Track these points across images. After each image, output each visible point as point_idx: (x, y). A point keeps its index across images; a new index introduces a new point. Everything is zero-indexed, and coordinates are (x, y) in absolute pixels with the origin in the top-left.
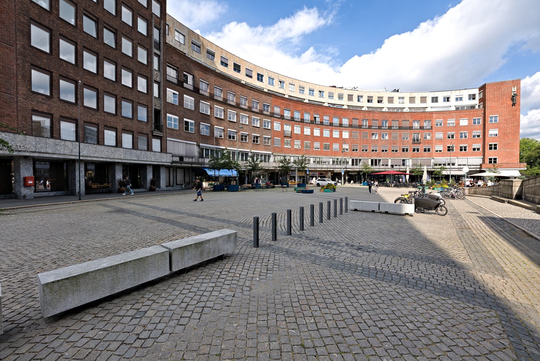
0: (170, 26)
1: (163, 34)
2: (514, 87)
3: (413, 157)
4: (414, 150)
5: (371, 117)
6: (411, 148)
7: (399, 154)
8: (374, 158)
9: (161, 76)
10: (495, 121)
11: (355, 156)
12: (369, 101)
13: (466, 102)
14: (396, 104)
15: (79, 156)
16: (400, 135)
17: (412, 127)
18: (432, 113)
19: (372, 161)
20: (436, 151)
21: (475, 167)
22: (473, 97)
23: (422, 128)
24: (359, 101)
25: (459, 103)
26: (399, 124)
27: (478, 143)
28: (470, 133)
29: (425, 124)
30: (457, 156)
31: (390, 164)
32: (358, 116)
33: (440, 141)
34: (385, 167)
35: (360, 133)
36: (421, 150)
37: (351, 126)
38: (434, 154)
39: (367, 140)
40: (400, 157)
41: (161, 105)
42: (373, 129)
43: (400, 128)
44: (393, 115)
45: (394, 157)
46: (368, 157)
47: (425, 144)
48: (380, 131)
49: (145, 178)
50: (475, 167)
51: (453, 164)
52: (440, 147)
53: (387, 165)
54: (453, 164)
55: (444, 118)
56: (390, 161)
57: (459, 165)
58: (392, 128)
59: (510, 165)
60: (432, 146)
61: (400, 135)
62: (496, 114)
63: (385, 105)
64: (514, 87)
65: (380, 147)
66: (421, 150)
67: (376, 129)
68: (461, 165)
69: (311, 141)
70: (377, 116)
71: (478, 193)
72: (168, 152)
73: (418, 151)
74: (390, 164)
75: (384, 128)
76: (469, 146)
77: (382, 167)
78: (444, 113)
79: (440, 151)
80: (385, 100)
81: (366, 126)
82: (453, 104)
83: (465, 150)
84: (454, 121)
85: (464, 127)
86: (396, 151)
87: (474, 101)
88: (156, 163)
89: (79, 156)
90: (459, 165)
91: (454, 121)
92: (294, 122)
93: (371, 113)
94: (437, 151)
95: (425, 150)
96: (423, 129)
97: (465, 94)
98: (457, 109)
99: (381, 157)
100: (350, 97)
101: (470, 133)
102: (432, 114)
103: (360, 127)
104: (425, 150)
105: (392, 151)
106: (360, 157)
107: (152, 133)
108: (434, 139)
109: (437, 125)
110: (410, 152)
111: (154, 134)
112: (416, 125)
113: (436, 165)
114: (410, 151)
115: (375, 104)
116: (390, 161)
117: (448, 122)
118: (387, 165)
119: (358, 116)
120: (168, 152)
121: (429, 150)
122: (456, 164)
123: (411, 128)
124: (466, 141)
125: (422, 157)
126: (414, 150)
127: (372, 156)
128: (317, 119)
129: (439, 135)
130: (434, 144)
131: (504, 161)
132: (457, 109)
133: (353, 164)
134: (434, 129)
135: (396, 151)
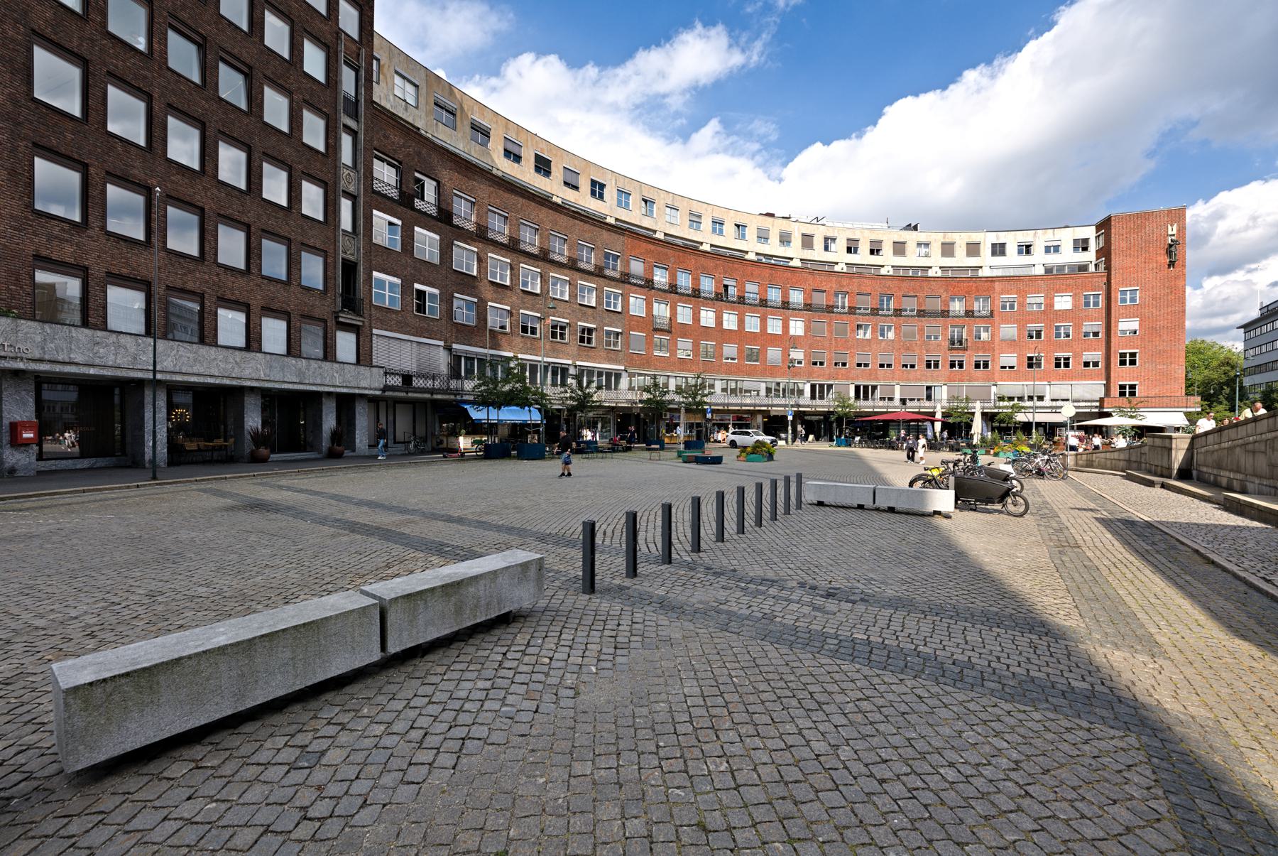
0: (382, 62)
1: (366, 81)
2: (1172, 225)
3: (950, 380)
4: (952, 365)
8: (862, 383)
9: (359, 181)
10: (1133, 300)
13: (1069, 256)
14: (912, 258)
15: (155, 371)
16: (921, 330)
18: (991, 280)
20: (1002, 367)
21: (1089, 404)
23: (969, 314)
24: (826, 249)
25: (1053, 259)
26: (919, 304)
27: (1095, 350)
28: (1078, 326)
29: (977, 306)
30: (1047, 378)
31: (897, 396)
33: (1011, 344)
34: (886, 403)
35: (829, 324)
38: (997, 375)
40: (920, 380)
41: (359, 250)
43: (922, 313)
45: (908, 380)
47: (977, 350)
48: (874, 319)
50: (1089, 404)
52: (1009, 359)
53: (891, 399)
54: (1041, 398)
55: (1019, 292)
56: (897, 388)
57: (1052, 400)
61: (921, 330)
62: (1134, 285)
63: (887, 260)
64: (1172, 225)
65: (875, 357)
69: (716, 341)
70: (867, 286)
74: (897, 396)
75: (885, 312)
76: (1074, 357)
77: (881, 403)
78: (1020, 281)
79: (1010, 367)
83: (1067, 365)
84: (1042, 300)
85: (1064, 314)
86: (912, 366)
87: (1085, 253)
88: (345, 390)
89: (155, 371)
90: (1052, 400)
91: (1042, 300)
94: (1005, 367)
95: (977, 366)
97: (1066, 237)
98: (1049, 270)
99: (877, 379)
100: (807, 241)
101: (1078, 326)
102: (992, 281)
103: (830, 309)
104: (977, 366)
105: (904, 366)
106: (829, 379)
107: (337, 317)
108: (997, 340)
109: (1004, 307)
110: (944, 368)
111: (341, 319)
112: (957, 307)
113: (1001, 399)
115: (863, 257)
117: (1028, 301)
118: (891, 399)
122: (1047, 398)
123: (945, 314)
127: (857, 378)
129: (1009, 331)
130: (996, 352)
132: (1049, 270)
133: (813, 397)
134: (996, 318)
135: (912, 366)
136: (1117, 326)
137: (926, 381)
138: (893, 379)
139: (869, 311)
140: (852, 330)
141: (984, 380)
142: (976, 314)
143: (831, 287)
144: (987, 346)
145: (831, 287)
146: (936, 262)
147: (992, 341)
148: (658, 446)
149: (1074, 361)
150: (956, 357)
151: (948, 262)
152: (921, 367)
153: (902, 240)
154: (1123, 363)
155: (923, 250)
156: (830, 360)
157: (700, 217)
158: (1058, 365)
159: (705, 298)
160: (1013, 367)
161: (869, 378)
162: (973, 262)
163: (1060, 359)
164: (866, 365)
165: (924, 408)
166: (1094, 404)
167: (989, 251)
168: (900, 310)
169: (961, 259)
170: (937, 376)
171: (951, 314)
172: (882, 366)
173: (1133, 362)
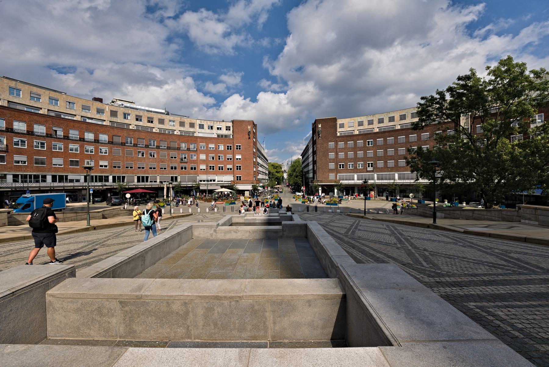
3: (181, 174)
4: (182, 168)
5: (137, 135)
6: (179, 166)
7: (167, 171)
8: (141, 175)
11: (117, 173)
12: (137, 120)
13: (224, 132)
14: (167, 126)
15: (2, 180)
16: (169, 155)
17: (180, 148)
18: (197, 137)
19: (139, 178)
20: (201, 169)
21: (228, 183)
22: (228, 128)
23: (188, 149)
24: (125, 118)
25: (219, 132)
26: (168, 144)
28: (225, 156)
29: (192, 147)
30: (216, 174)
31: (158, 181)
32: (119, 133)
33: (203, 162)
34: (153, 183)
35: (123, 151)
36: (188, 169)
37: (111, 143)
38: (199, 172)
39: (132, 158)
40: (168, 174)
42: (139, 147)
43: (169, 148)
44: (161, 136)
45: (163, 174)
46: (133, 174)
47: (191, 163)
48: (147, 149)
49: (307, 135)
50: (228, 183)
51: (214, 181)
52: (203, 167)
53: (156, 182)
54: (214, 181)
56: (158, 177)
57: (218, 181)
58: (161, 147)
59: (247, 181)
60: (197, 165)
61: (169, 155)
63: (156, 127)
65: (147, 165)
66: (188, 169)
67: (142, 147)
68: (219, 181)
69: (47, 156)
70: (142, 135)
71: (514, 221)
72: (366, 201)
73: (185, 168)
74: (158, 181)
75: (152, 147)
76: (224, 167)
77: (151, 183)
79: (204, 170)
80: (156, 121)
81: (131, 143)
82: (214, 133)
83: (222, 169)
84: (214, 146)
86: (165, 169)
87: (230, 131)
90: (218, 181)
91: (214, 146)
92: (13, 134)
93: (136, 132)
94: (202, 169)
95: (192, 169)
96: (190, 150)
97: (223, 125)
98: (218, 136)
99: (148, 174)
100: (114, 114)
101: (225, 156)
102: (196, 138)
103: (123, 144)
104: (192, 169)
105: (161, 168)
106: (123, 174)
108: (198, 160)
109: (201, 148)
110: (179, 169)
112: (183, 145)
113: (201, 181)
114: (178, 169)
115: (144, 123)
116: (158, 177)
118: (156, 182)
119: (119, 133)
120: (366, 201)
121: (195, 169)
122: (216, 181)
123: (179, 149)
124: (222, 163)
125: (189, 174)
126: (182, 168)
127: (138, 173)
128: (58, 133)
129: (203, 157)
130: (199, 164)
131: (246, 179)
132: (218, 136)
134: (198, 152)
135: (165, 169)
136: (235, 157)
137: (171, 175)
138: (156, 174)
139: (144, 146)
140: (135, 153)
141: (194, 174)
142: (191, 150)
143: (123, 135)
144: (194, 162)
145: (123, 135)
146: (178, 130)
147: (197, 160)
148: (370, 210)
149: (224, 168)
150: (184, 165)
151: (182, 129)
152: (168, 169)
153: (162, 118)
154: (237, 169)
155: (172, 123)
156: (123, 166)
157: (40, 95)
158: (219, 169)
159: (37, 135)
160: (205, 170)
161: (145, 173)
162: (192, 130)
163: (220, 167)
164: (143, 168)
165: (153, 185)
166: (229, 183)
167: (198, 127)
168: (158, 146)
169: (187, 128)
170: (176, 172)
171: (181, 149)
172: (151, 168)
173: (240, 169)
